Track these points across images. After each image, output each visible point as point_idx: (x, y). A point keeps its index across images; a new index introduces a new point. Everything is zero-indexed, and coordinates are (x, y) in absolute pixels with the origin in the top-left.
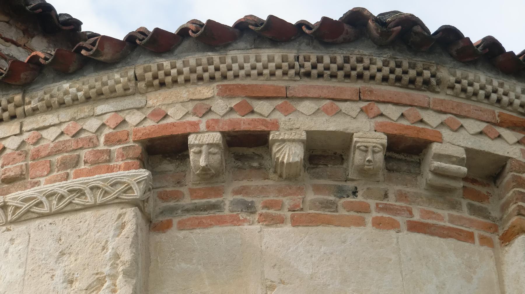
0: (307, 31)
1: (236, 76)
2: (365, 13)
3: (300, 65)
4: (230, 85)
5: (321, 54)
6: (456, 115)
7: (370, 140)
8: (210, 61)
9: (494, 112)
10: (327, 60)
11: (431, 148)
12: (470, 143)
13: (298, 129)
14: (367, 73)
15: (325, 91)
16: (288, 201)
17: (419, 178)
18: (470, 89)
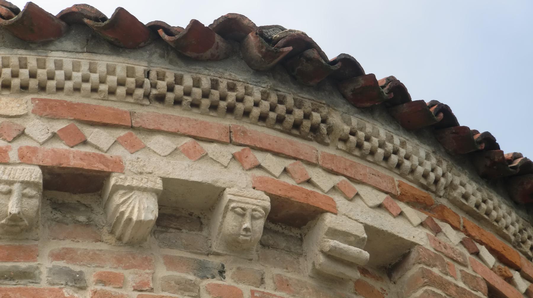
0: (166, 37)
1: (60, 89)
2: (245, 22)
3: (151, 84)
4: (50, 100)
5: (180, 73)
6: (349, 178)
7: (248, 200)
8: (23, 62)
9: (393, 180)
10: (188, 81)
11: (324, 220)
12: (369, 219)
13: (151, 173)
14: (240, 107)
15: (183, 124)
16: (131, 276)
17: (301, 260)
18: (366, 144)
